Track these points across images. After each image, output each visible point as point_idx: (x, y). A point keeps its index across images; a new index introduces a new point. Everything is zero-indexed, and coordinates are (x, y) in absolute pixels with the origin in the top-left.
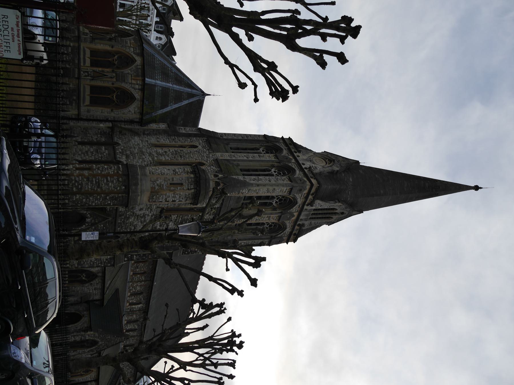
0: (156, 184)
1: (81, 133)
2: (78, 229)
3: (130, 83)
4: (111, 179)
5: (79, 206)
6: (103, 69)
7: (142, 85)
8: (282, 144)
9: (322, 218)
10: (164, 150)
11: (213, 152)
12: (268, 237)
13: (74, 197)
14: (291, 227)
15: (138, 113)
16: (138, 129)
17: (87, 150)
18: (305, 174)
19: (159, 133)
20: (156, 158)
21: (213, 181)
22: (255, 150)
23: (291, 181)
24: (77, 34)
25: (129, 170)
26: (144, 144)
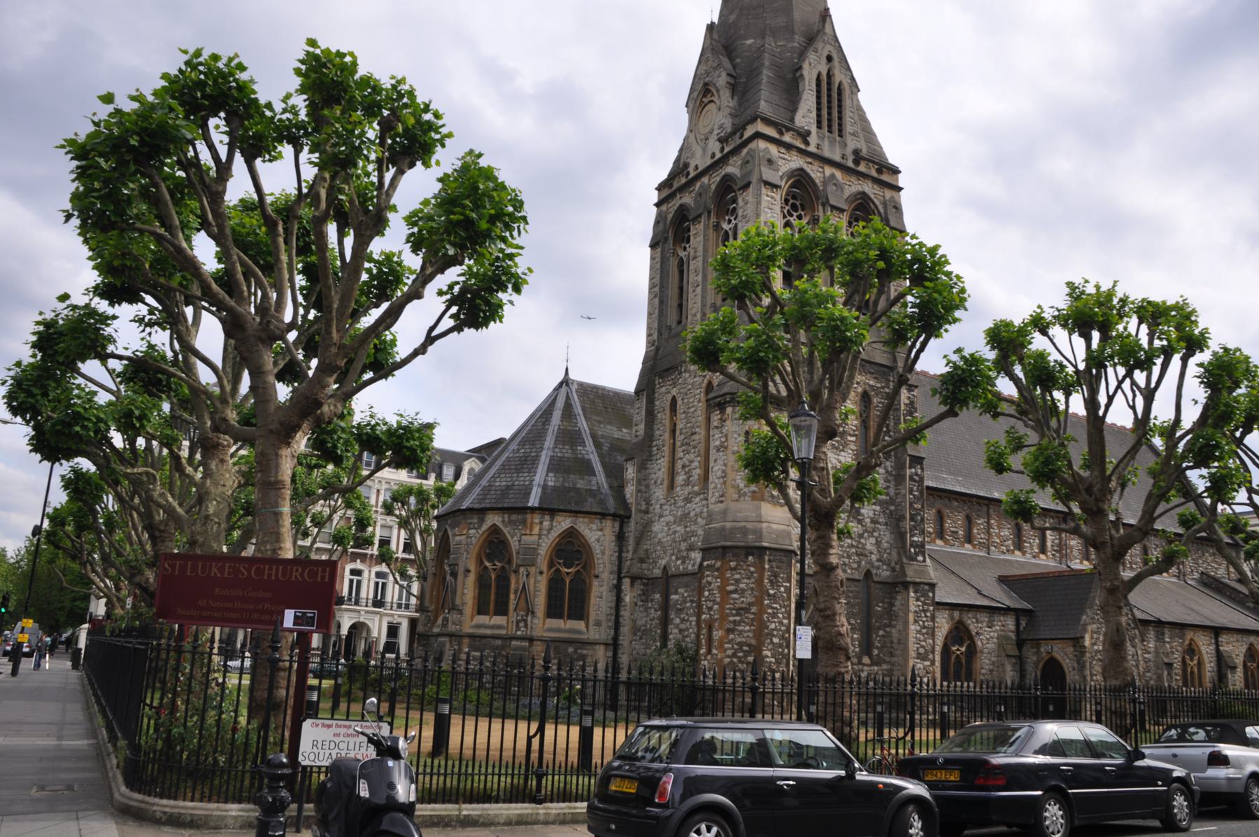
0: (746, 490)
3: (540, 538)
4: (732, 584)
6: (512, 591)
7: (544, 514)
9: (840, 106)
13: (768, 660)
17: (676, 631)
20: (696, 488)
23: (747, 185)
24: (446, 639)
25: (713, 545)
26: (667, 512)
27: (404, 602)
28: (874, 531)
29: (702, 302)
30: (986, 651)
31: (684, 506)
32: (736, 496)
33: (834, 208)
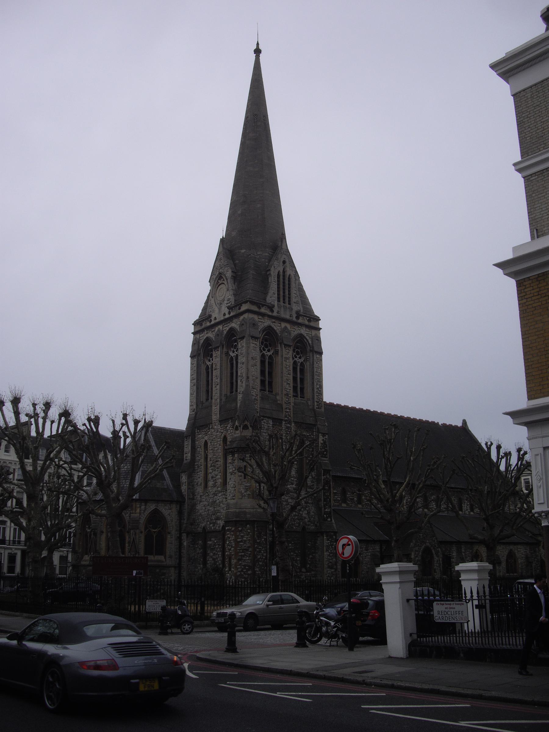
0: (245, 494)
1: (194, 564)
2: (292, 568)
3: (140, 515)
4: (240, 538)
5: (267, 568)
8: (201, 335)
10: (210, 479)
11: (212, 424)
12: (311, 355)
13: (257, 572)
14: (299, 328)
15: (170, 505)
16: (188, 505)
17: (211, 559)
18: (237, 316)
19: (191, 482)
20: (219, 489)
21: (242, 431)
22: (209, 371)
27: (17, 539)
28: (306, 507)
29: (220, 393)
30: (364, 562)
31: (213, 497)
32: (240, 497)
33: (286, 345)
